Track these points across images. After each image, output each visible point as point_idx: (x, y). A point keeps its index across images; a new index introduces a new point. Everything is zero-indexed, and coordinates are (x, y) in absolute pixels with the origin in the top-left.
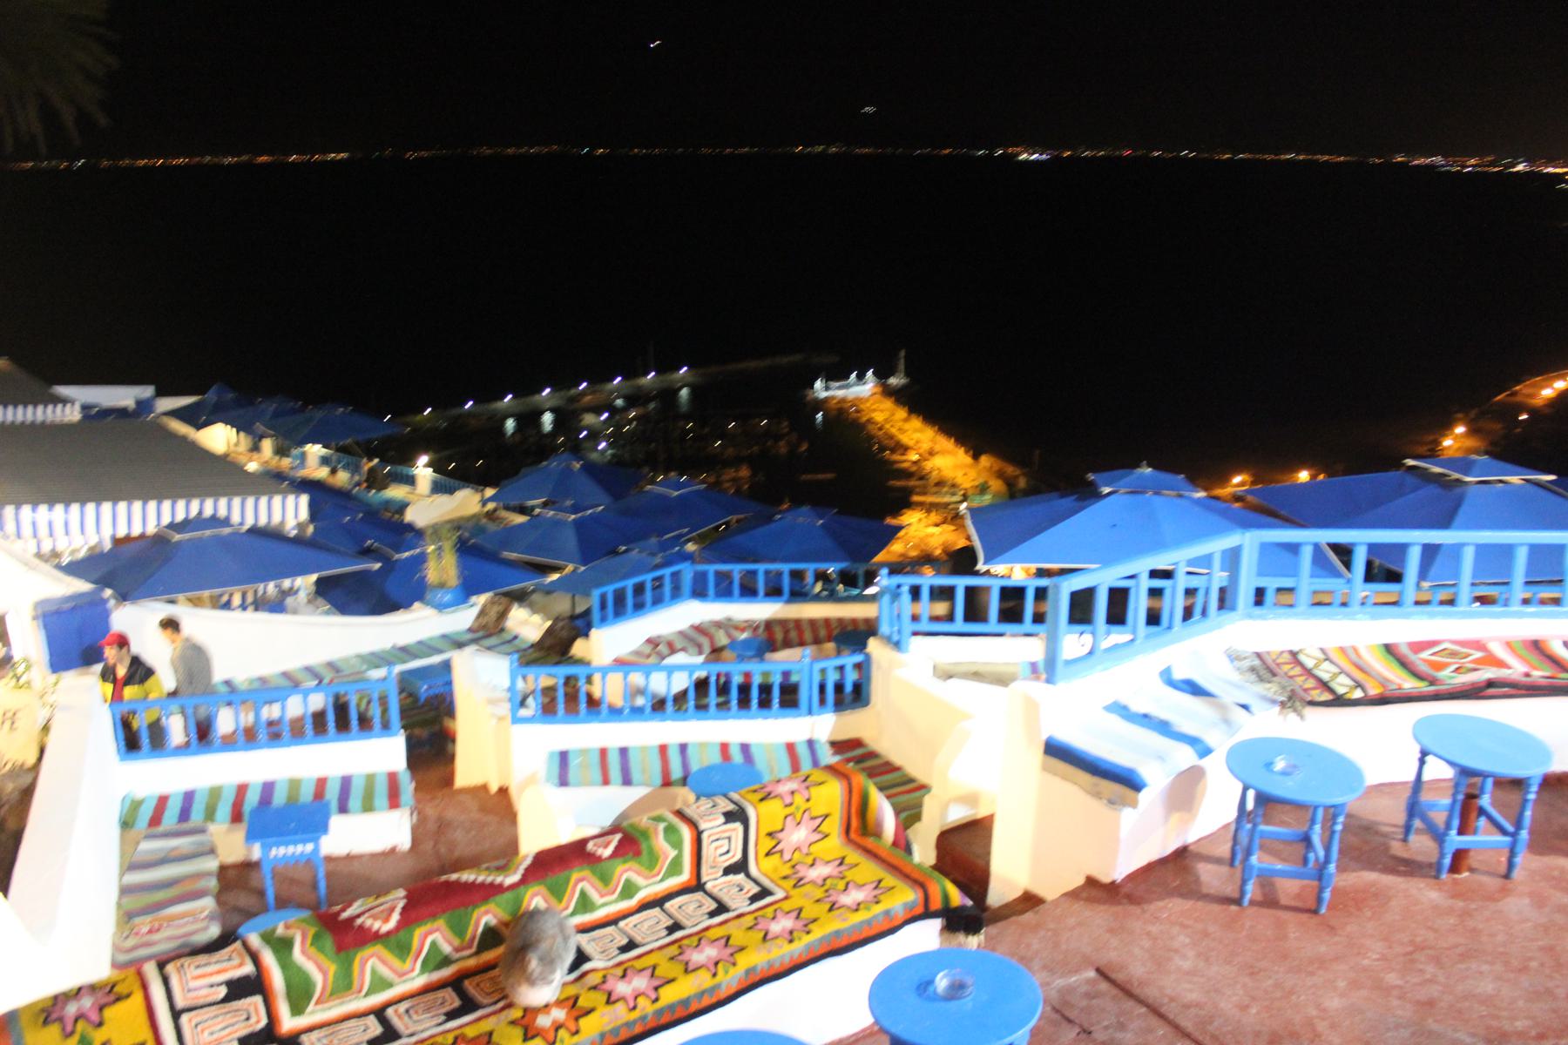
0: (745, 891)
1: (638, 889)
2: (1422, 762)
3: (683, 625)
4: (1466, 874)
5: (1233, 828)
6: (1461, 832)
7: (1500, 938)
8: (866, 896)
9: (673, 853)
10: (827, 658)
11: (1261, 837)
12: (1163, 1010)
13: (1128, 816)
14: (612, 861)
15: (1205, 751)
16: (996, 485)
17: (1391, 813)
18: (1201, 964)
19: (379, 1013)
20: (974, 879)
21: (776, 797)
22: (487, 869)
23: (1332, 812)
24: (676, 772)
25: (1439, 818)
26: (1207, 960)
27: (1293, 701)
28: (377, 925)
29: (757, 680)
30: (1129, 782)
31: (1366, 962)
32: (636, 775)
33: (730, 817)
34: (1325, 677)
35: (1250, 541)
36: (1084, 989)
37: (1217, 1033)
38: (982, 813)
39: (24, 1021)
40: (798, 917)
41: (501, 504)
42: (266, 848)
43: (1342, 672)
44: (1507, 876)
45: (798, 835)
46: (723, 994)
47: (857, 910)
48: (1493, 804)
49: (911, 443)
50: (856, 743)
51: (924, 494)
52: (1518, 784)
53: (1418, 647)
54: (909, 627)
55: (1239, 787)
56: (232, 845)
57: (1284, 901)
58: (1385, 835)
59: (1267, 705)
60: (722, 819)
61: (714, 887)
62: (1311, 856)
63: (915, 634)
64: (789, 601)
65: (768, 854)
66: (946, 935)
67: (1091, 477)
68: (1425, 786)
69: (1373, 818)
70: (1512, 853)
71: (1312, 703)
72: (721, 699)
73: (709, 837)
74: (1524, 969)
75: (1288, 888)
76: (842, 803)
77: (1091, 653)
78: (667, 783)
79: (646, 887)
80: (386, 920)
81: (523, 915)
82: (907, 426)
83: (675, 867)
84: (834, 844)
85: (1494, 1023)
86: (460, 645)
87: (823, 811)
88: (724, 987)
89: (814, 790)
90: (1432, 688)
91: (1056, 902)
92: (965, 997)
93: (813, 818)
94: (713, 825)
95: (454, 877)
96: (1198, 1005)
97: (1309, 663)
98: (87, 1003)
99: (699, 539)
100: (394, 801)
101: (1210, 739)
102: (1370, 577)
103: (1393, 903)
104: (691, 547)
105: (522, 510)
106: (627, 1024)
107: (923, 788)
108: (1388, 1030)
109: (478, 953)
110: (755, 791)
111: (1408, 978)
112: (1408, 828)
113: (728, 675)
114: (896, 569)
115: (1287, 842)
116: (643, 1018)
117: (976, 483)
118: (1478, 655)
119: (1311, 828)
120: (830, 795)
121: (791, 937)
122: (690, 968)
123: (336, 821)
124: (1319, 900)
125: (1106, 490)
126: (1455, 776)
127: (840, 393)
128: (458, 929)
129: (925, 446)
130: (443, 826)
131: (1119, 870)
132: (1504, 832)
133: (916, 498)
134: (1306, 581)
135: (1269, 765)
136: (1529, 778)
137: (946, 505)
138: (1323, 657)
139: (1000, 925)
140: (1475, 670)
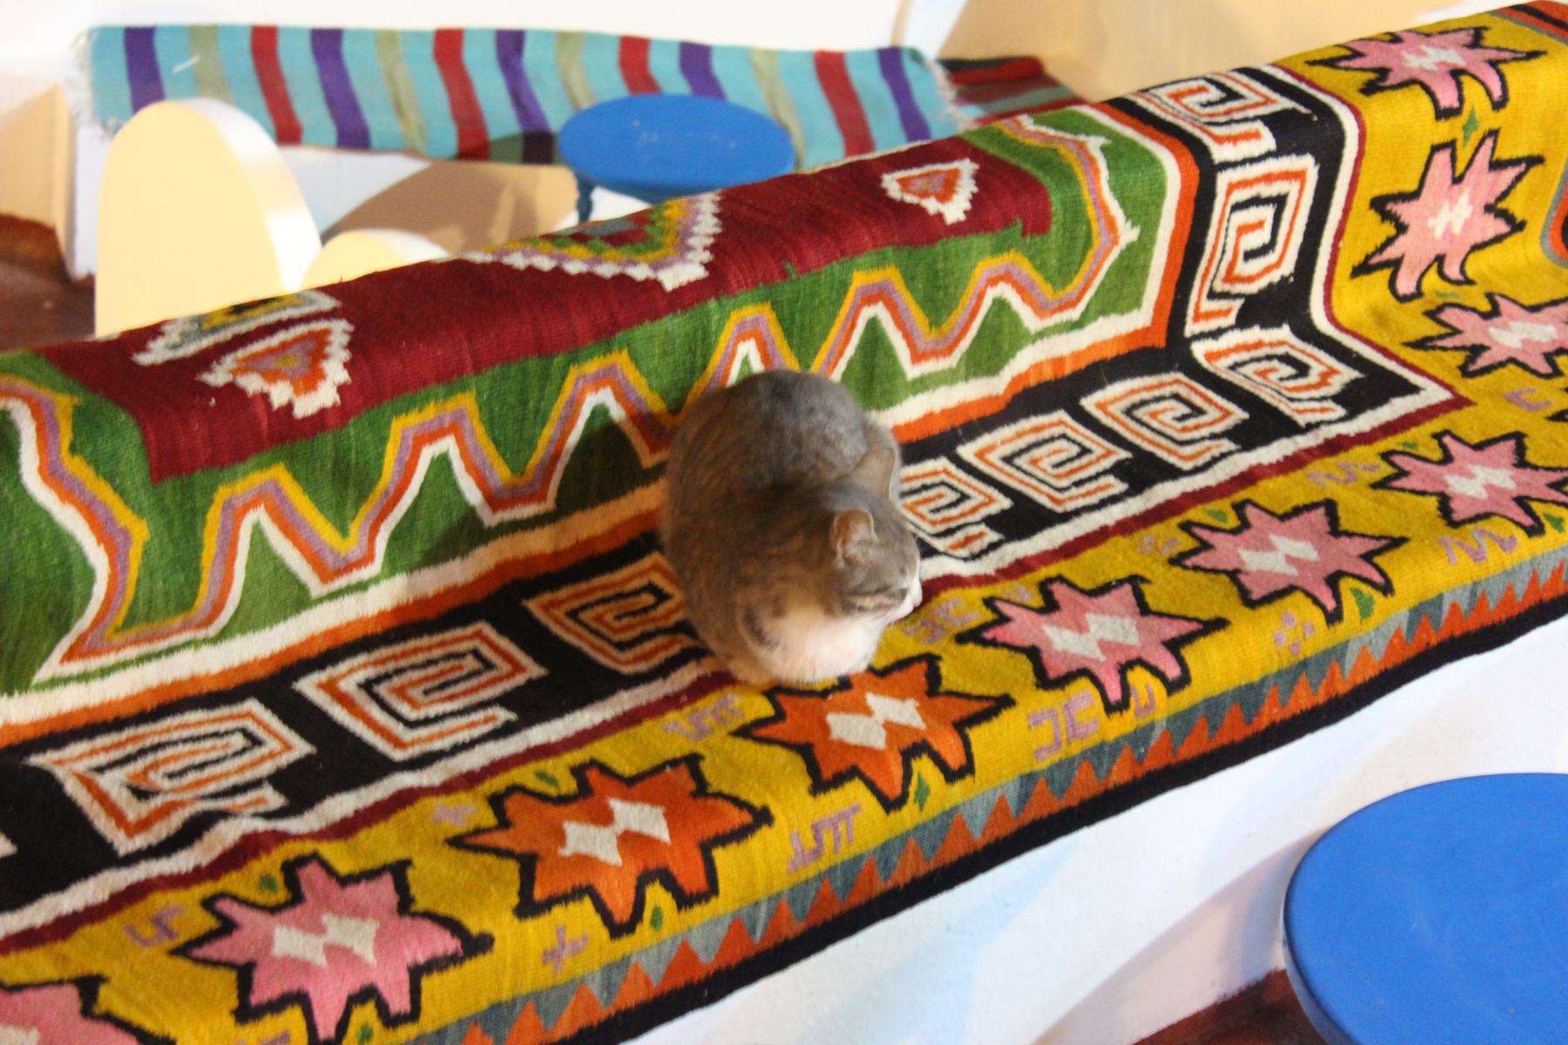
0: (1313, 378)
1: (1020, 338)
9: (1128, 234)
24: (501, 120)
28: (280, 394)
32: (377, 119)
46: (1349, 675)
60: (1268, 142)
61: (1211, 356)
65: (1363, 269)
73: (1231, 188)
78: (475, 147)
80: (310, 379)
93: (1496, 165)
106: (1100, 753)
116: (1140, 736)
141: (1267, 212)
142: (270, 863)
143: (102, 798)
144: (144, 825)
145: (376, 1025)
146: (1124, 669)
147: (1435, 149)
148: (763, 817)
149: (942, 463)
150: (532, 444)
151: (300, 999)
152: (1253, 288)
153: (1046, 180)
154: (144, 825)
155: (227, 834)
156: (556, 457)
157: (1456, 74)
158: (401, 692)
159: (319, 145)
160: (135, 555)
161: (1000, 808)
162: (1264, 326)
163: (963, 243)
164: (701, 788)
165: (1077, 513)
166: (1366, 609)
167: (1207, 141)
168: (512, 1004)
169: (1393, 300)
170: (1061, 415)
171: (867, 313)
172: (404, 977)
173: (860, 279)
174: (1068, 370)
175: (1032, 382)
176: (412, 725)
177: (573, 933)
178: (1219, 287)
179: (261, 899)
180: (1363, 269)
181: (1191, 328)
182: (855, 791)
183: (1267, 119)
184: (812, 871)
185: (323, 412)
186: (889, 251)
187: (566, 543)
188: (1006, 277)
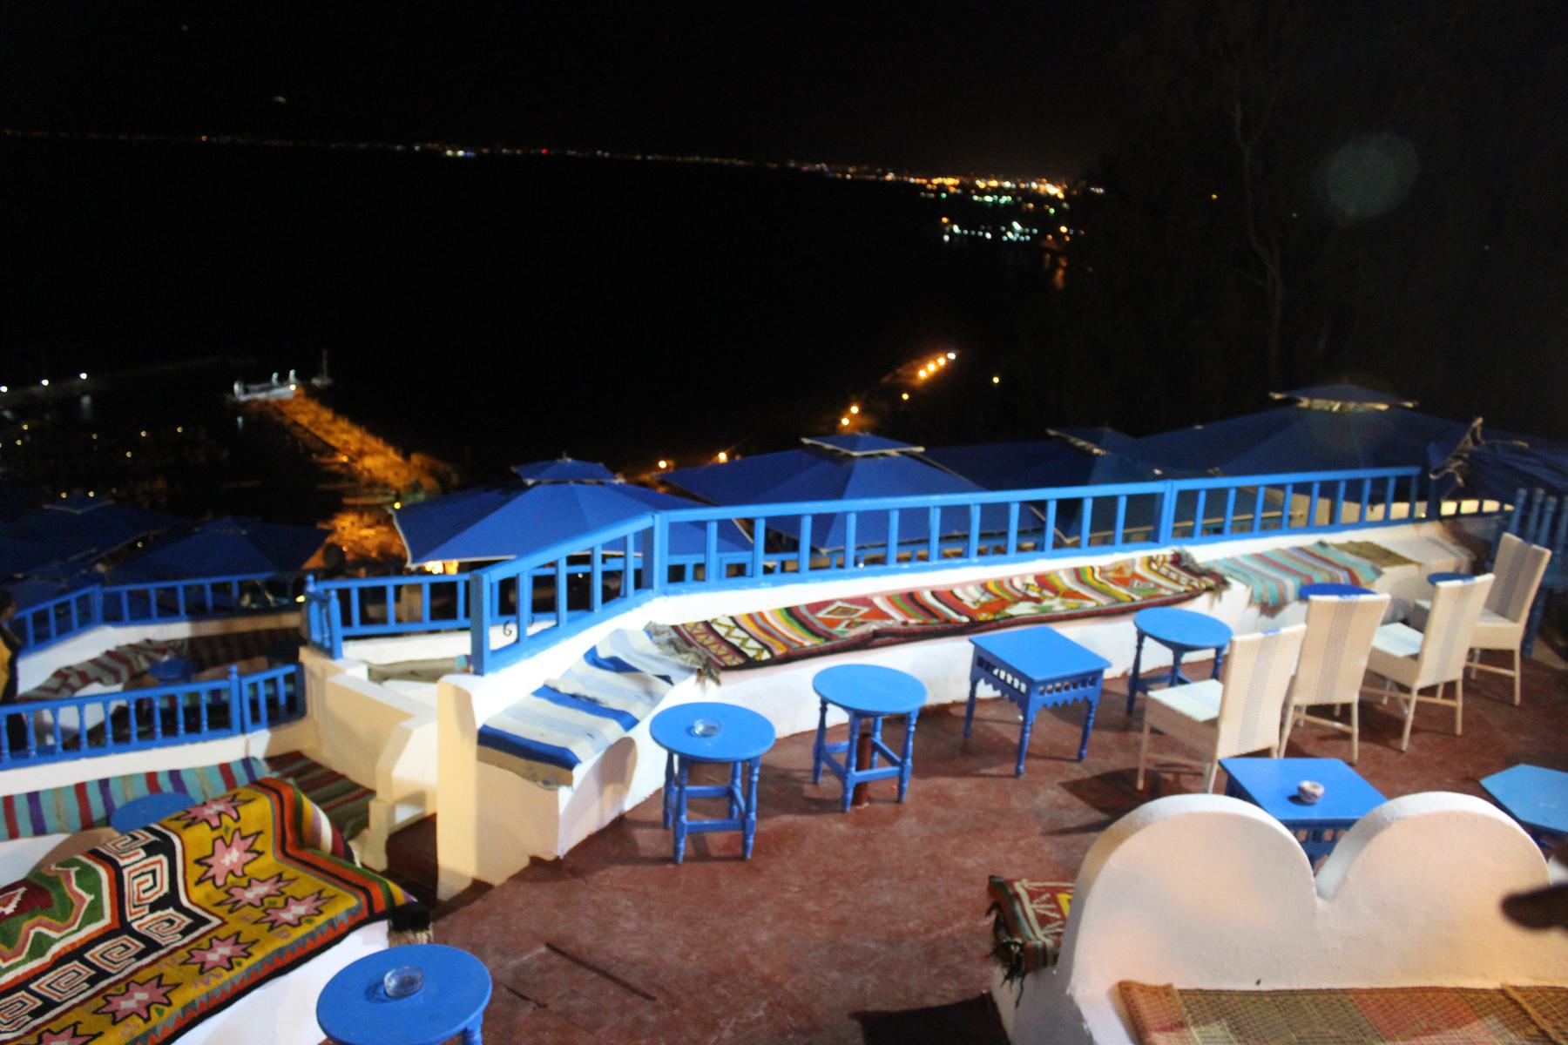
1: (53, 942)
2: (824, 710)
4: (866, 804)
5: (663, 791)
6: (859, 768)
8: (307, 910)
9: (89, 898)
10: (257, 671)
11: (688, 797)
12: (613, 971)
13: (564, 795)
14: (19, 918)
15: (629, 722)
16: (429, 483)
17: (802, 759)
21: (201, 821)
23: (749, 764)
25: (841, 759)
27: (709, 669)
29: (182, 702)
30: (562, 761)
31: (788, 896)
32: (50, 822)
33: (151, 849)
34: (737, 642)
35: (659, 522)
38: (429, 812)
43: (751, 636)
44: (899, 801)
45: (232, 857)
47: (300, 924)
48: (883, 740)
50: (297, 756)
51: (356, 495)
52: (901, 720)
53: (816, 607)
54: (339, 630)
55: (664, 754)
57: (714, 852)
58: (798, 780)
59: (683, 674)
60: (143, 854)
61: (140, 926)
62: (735, 808)
63: (347, 638)
67: (514, 469)
68: (828, 732)
70: (901, 780)
72: (144, 729)
73: (130, 873)
74: (915, 878)
75: (717, 840)
76: (274, 818)
77: (517, 641)
78: (88, 824)
79: (62, 938)
82: (333, 428)
83: (94, 912)
84: (269, 861)
85: (893, 928)
87: (253, 830)
88: (159, 1030)
89: (243, 810)
90: (828, 644)
91: (503, 887)
92: (415, 992)
93: (244, 838)
94: (134, 861)
97: (722, 631)
99: (111, 559)
102: (771, 548)
104: (100, 568)
107: (371, 793)
108: (810, 951)
110: (178, 819)
112: (816, 771)
113: (150, 701)
115: (716, 799)
117: (407, 483)
118: (865, 610)
119: (733, 783)
120: (260, 811)
121: (230, 963)
124: (745, 846)
126: (850, 719)
127: (261, 396)
129: (354, 447)
132: (893, 762)
133: (347, 501)
134: (715, 559)
135: (690, 730)
136: (909, 713)
137: (379, 507)
139: (449, 917)
140: (863, 623)
147: (214, 840)
152: (152, 900)
153: (49, 888)
157: (219, 814)
163: (14, 919)
165: (66, 1001)
166: (160, 1013)
169: (214, 888)
170: (76, 962)
174: (78, 946)
175: (63, 953)
178: (136, 903)
180: (199, 882)
181: (129, 919)
188: (39, 924)
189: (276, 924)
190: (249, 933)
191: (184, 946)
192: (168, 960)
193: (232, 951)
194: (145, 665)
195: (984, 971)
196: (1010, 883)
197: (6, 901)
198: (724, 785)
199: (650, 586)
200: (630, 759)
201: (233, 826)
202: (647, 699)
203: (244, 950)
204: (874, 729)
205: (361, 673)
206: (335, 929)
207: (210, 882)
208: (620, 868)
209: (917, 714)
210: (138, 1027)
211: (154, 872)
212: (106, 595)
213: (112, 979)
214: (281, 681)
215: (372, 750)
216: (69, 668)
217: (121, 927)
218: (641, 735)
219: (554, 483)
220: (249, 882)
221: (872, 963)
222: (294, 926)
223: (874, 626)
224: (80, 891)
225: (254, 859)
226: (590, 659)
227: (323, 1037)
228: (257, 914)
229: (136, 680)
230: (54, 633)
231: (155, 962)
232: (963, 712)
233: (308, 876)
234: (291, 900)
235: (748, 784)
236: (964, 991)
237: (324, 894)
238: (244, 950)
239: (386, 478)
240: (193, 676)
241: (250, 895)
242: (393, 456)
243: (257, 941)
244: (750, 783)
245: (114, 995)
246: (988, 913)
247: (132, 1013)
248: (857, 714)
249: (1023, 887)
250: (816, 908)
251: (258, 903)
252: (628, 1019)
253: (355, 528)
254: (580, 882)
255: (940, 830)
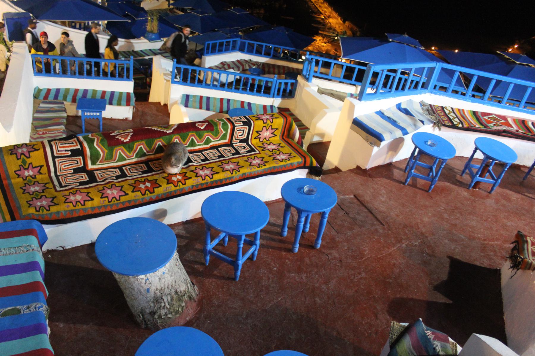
1: (211, 141)
2: (475, 152)
3: (234, 60)
5: (408, 160)
7: (482, 210)
9: (224, 132)
12: (373, 211)
13: (376, 149)
15: (406, 133)
16: (349, 33)
17: (460, 166)
18: (388, 200)
19: (120, 168)
20: (321, 160)
22: (161, 127)
23: (442, 161)
24: (225, 108)
25: (475, 171)
26: (390, 199)
27: (438, 124)
28: (122, 139)
30: (379, 138)
32: (211, 107)
33: (245, 123)
34: (451, 118)
36: (349, 200)
37: (388, 221)
38: (325, 140)
39: (4, 152)
40: (262, 160)
41: (175, 7)
42: (83, 112)
43: (457, 117)
44: (490, 193)
45: (266, 134)
46: (233, 180)
47: (282, 161)
48: (492, 170)
49: (323, 12)
50: (287, 110)
51: (323, 31)
55: (413, 147)
56: (72, 110)
57: (418, 186)
58: (455, 172)
60: (242, 124)
62: (431, 174)
63: (314, 76)
64: (272, 58)
65: (255, 138)
66: (309, 175)
69: (454, 166)
70: (494, 186)
71: (445, 125)
73: (237, 128)
74: (486, 220)
75: (421, 182)
76: (283, 126)
78: (221, 111)
79: (214, 141)
80: (126, 138)
81: (172, 144)
82: (322, 5)
84: (277, 139)
85: (472, 234)
86: (155, 54)
89: (274, 120)
90: (485, 129)
91: (345, 172)
93: (272, 129)
94: (239, 125)
95: (150, 128)
96: (384, 212)
97: (447, 112)
98: (25, 150)
99: (243, 32)
100: (128, 104)
101: (408, 130)
103: (452, 194)
104: (240, 33)
105: (183, 10)
106: (201, 184)
108: (440, 230)
109: (156, 153)
111: (451, 217)
112: (463, 172)
114: (311, 53)
116: (207, 183)
118: (503, 121)
119: (433, 165)
120: (279, 122)
121: (259, 166)
122: (224, 170)
123: (108, 107)
124: (430, 188)
125: (391, 40)
128: (149, 145)
130: (144, 114)
131: (370, 165)
132: (493, 178)
133: (320, 32)
135: (426, 142)
136: (507, 163)
138: (452, 111)
139: (326, 175)
140: (501, 126)
141: (242, 131)
142: (110, 184)
143: (98, 176)
144: (101, 179)
145: (115, 200)
146: (205, 176)
148: (161, 186)
149: (200, 153)
150: (152, 147)
151: (107, 197)
152: (241, 139)
153: (214, 126)
154: (101, 179)
155: (108, 181)
156: (154, 148)
157: (267, 119)
158: (132, 170)
159: (204, 110)
160: (106, 153)
161: (189, 188)
162: (243, 143)
163: (203, 131)
164: (156, 183)
165: (211, 160)
166: (236, 173)
167: (235, 123)
168: (131, 200)
169: (259, 142)
171: (192, 137)
172: (119, 196)
173: (190, 134)
174: (217, 145)
176: (131, 173)
177: (137, 195)
178: (236, 138)
179: (108, 187)
180: (255, 138)
181: (233, 142)
182: (172, 185)
183: (242, 122)
184: (166, 192)
185: (127, 141)
186: (194, 131)
187: (155, 157)
188: (209, 135)
189: (275, 159)
190: (266, 159)
191: (247, 156)
192: (241, 158)
193: (260, 162)
194: (248, 68)
195: (500, 262)
196: (526, 236)
197: (202, 125)
198: (430, 165)
199: (427, 88)
200: (401, 145)
201: (270, 124)
202: (414, 127)
203: (264, 163)
204: (491, 165)
205: (316, 89)
206: (292, 166)
207: (259, 139)
208: (385, 179)
209: (510, 165)
210: (229, 175)
211: (243, 130)
212: (241, 42)
213: (225, 158)
214: (289, 84)
215: (312, 115)
216: (225, 62)
217: (230, 144)
218: (408, 138)
219: (399, 43)
220: (270, 143)
221: (461, 243)
222: (280, 161)
223: (505, 128)
224: (222, 129)
225: (273, 137)
226: (398, 107)
227: (280, 196)
228: (270, 154)
229: (244, 71)
230: (224, 50)
231: (237, 157)
232: (526, 170)
233: (288, 147)
234: (281, 153)
235: (439, 167)
236: (490, 265)
237: (292, 155)
238: (264, 163)
239: (335, 27)
240: (261, 75)
241: (269, 147)
242: (339, 20)
243: (268, 162)
244: (440, 167)
245: (224, 163)
246: (512, 243)
247: (229, 170)
248: (487, 157)
249: (530, 239)
250: (447, 217)
251: (271, 151)
252: (373, 228)
253: (320, 42)
254: (371, 179)
255: (501, 208)
